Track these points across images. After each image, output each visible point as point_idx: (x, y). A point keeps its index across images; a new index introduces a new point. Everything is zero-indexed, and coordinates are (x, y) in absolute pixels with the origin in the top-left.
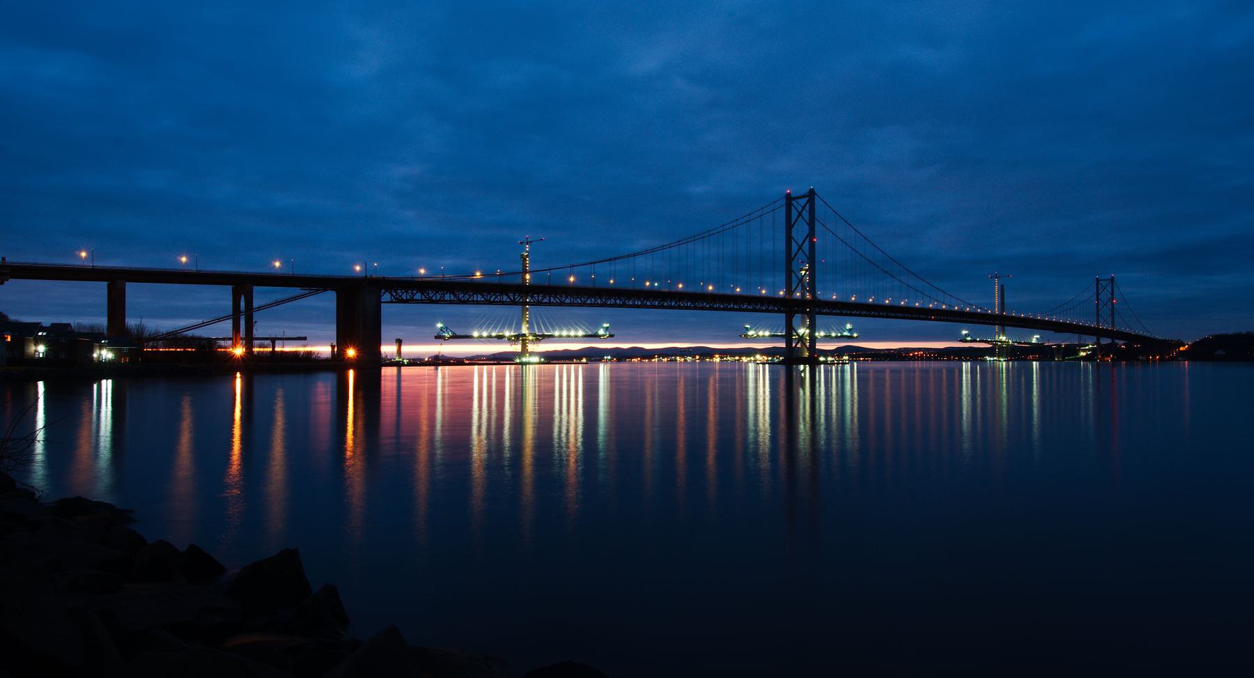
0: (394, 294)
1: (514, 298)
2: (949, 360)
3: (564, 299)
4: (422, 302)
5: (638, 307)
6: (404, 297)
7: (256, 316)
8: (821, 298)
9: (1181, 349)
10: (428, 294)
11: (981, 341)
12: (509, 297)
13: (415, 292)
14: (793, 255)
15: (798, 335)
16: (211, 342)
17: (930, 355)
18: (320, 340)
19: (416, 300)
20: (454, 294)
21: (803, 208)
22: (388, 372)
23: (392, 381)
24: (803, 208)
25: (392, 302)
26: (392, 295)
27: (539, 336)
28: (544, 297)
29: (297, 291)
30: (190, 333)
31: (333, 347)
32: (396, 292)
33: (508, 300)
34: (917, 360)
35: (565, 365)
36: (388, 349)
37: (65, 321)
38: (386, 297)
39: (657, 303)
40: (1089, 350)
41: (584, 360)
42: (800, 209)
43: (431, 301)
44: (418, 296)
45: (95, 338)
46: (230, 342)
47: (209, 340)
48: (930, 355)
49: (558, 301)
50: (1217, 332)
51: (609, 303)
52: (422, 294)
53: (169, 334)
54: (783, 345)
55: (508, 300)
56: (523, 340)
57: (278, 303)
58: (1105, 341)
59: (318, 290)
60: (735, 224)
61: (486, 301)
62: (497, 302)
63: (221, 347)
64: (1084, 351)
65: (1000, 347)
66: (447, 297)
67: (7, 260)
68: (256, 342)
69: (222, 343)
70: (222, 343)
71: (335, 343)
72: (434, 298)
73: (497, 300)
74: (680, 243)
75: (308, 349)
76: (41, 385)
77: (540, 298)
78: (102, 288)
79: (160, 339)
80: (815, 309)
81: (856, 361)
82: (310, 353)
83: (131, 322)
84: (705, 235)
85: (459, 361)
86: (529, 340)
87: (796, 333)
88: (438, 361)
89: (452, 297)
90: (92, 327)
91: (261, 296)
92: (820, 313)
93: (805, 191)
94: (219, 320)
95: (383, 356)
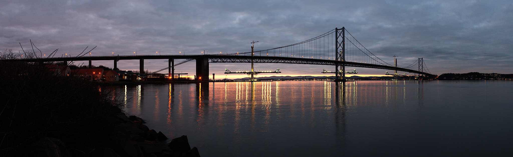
0: (212, 60)
1: (249, 60)
2: (383, 80)
3: (265, 60)
4: (221, 62)
5: (289, 63)
6: (215, 61)
7: (175, 67)
8: (346, 61)
9: (437, 77)
10: (222, 60)
11: (391, 75)
12: (247, 60)
13: (218, 59)
14: (338, 47)
15: (339, 72)
16: (163, 75)
17: (378, 78)
18: (192, 74)
19: (219, 62)
20: (231, 60)
21: (341, 33)
22: (211, 84)
23: (288, 56)
24: (341, 33)
25: (212, 62)
26: (212, 60)
27: (257, 72)
28: (259, 60)
29: (185, 60)
30: (158, 73)
31: (195, 76)
32: (213, 59)
33: (247, 61)
34: (374, 80)
35: (237, 82)
36: (211, 77)
37: (131, 70)
38: (210, 61)
39: (295, 62)
40: (417, 77)
41: (272, 80)
42: (340, 33)
43: (224, 62)
44: (219, 60)
45: (137, 74)
46: (168, 75)
47: (163, 74)
48: (378, 78)
49: (263, 61)
50: (443, 73)
51: (279, 62)
52: (221, 60)
53: (153, 73)
54: (335, 75)
55: (247, 61)
56: (252, 74)
57: (180, 64)
58: (421, 75)
59: (191, 60)
60: (320, 37)
61: (240, 61)
62: (244, 62)
63: (166, 76)
64: (416, 78)
65: (396, 77)
66: (228, 61)
67: (119, 55)
68: (175, 75)
69: (166, 75)
70: (166, 75)
71: (196, 75)
72: (224, 61)
73: (244, 61)
74: (303, 43)
75: (188, 77)
76: (126, 86)
77: (257, 60)
78: (138, 61)
79: (151, 74)
80: (344, 64)
81: (357, 80)
82: (189, 78)
83: (145, 70)
84: (310, 40)
85: (232, 81)
86: (254, 74)
87: (339, 71)
88: (225, 80)
89: (230, 60)
90: (136, 71)
91: (176, 61)
92: (346, 66)
93: (342, 27)
94: (165, 69)
95: (209, 79)
